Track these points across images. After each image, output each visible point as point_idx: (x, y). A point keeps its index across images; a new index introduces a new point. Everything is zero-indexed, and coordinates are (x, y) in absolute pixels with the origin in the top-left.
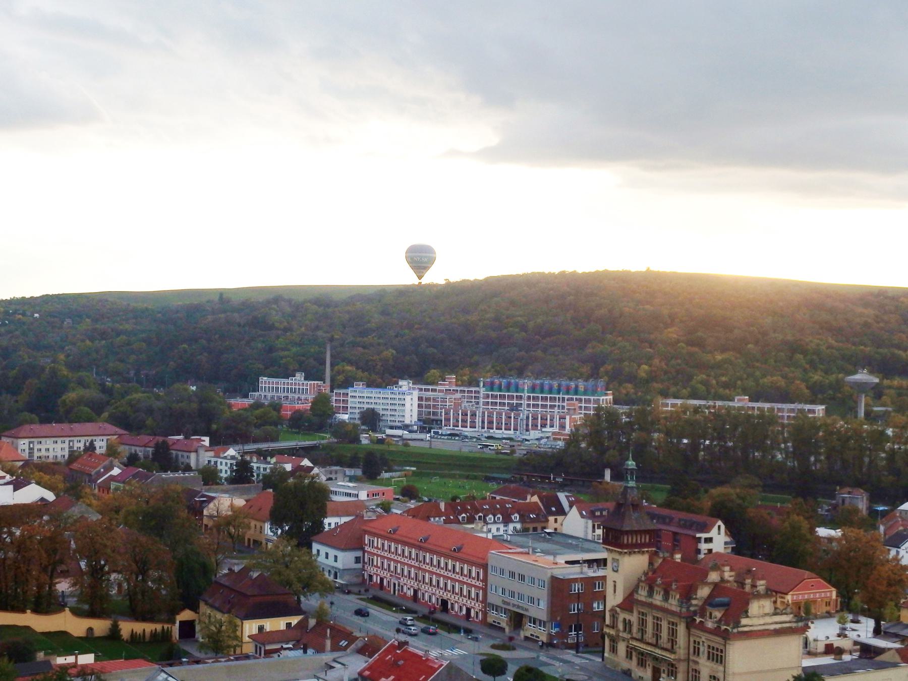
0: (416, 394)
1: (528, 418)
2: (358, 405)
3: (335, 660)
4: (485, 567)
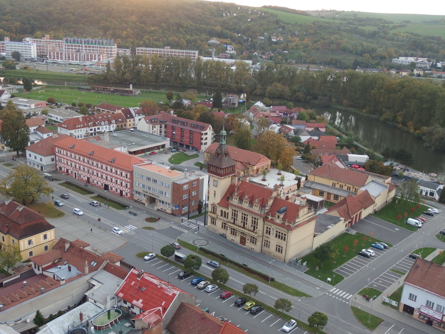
0: (35, 44)
1: (85, 55)
2: (10, 50)
3: (92, 278)
4: (132, 173)
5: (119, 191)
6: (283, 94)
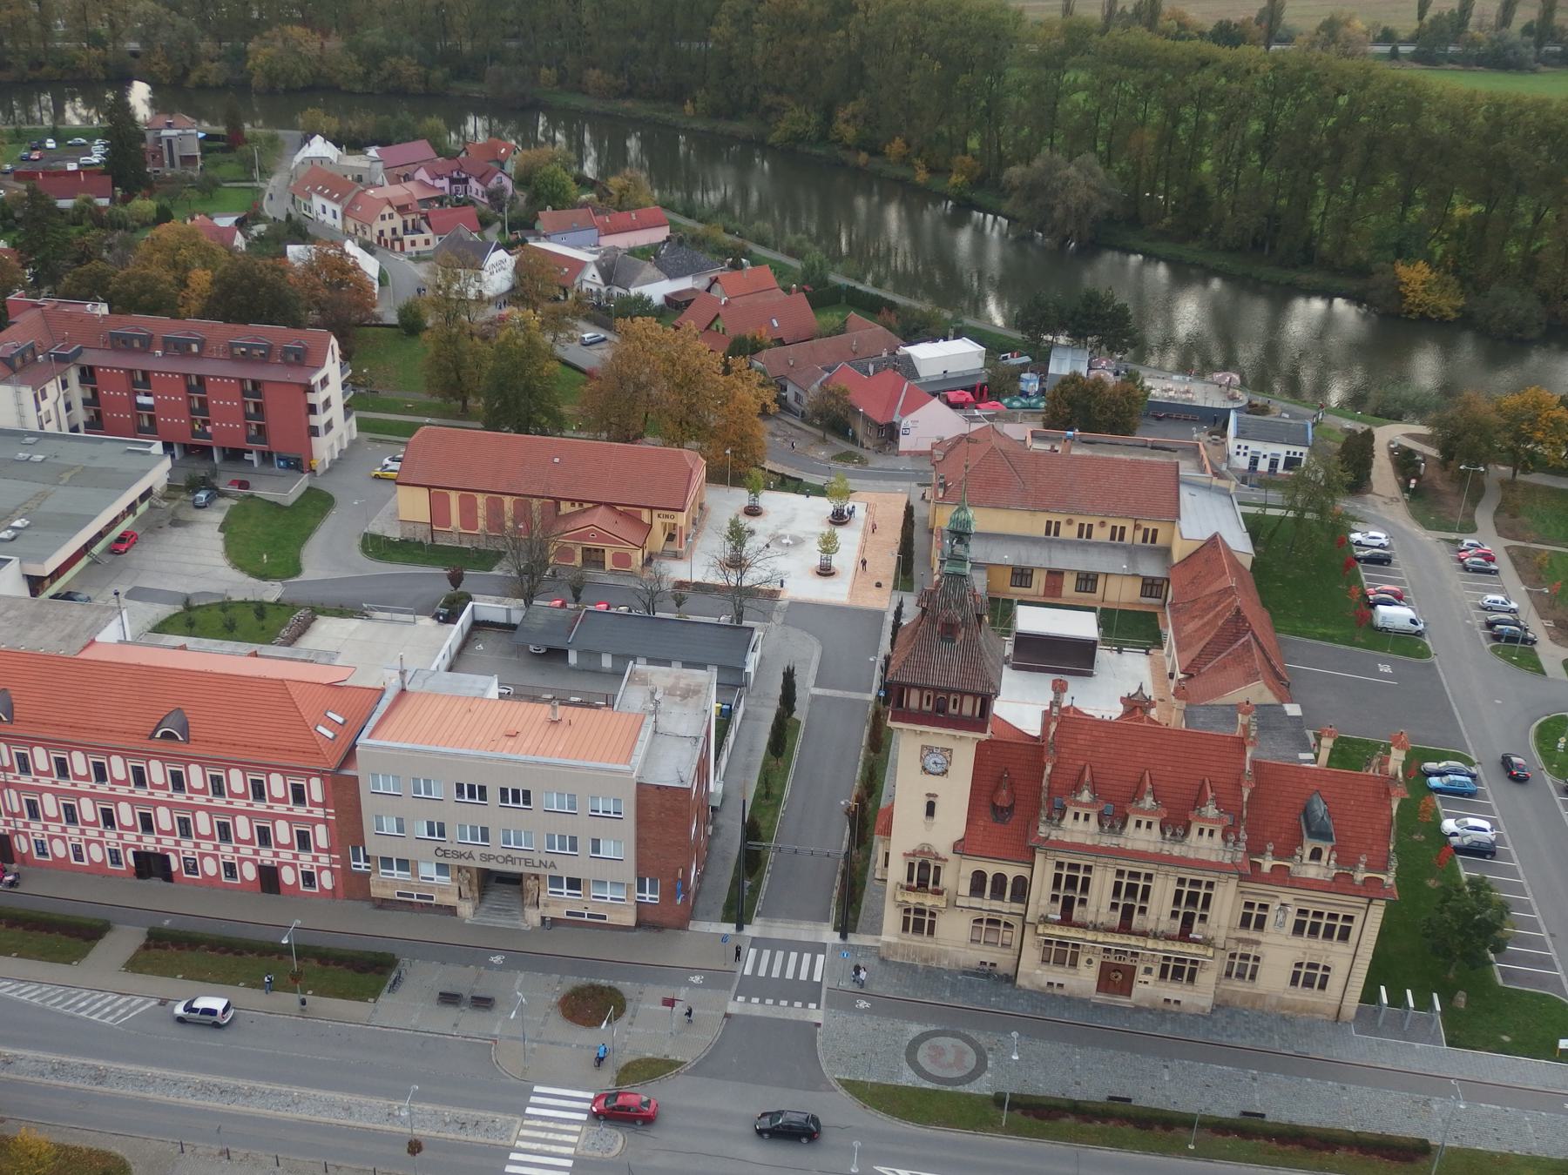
5: (250, 872)
6: (324, 69)
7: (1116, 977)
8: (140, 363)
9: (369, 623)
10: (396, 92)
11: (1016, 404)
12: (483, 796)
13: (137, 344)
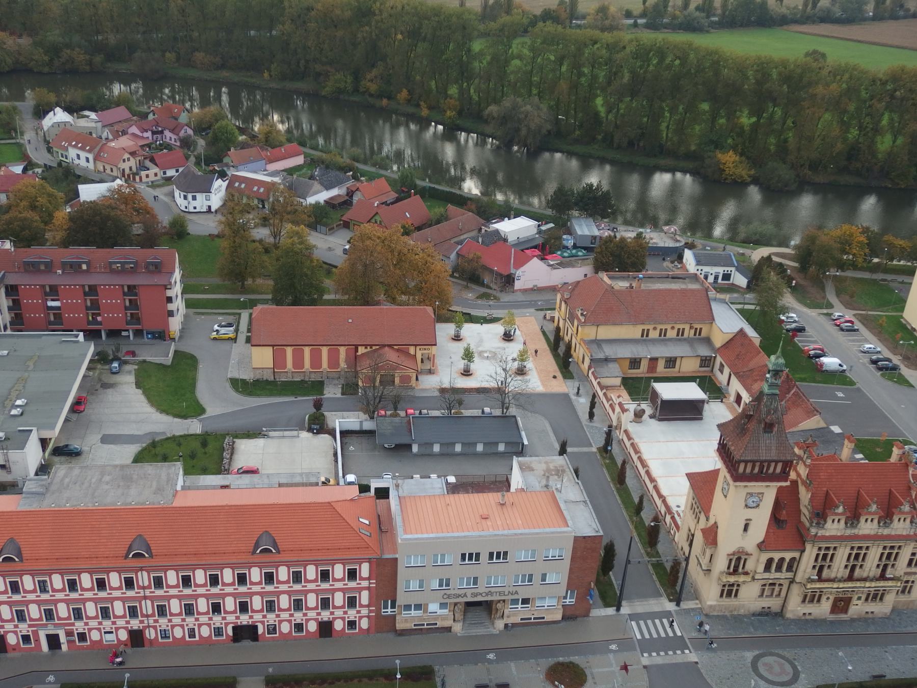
6: (21, 59)
7: (841, 604)
8: (48, 280)
9: (269, 440)
10: (71, 72)
11: (566, 254)
12: (477, 559)
13: (42, 267)
